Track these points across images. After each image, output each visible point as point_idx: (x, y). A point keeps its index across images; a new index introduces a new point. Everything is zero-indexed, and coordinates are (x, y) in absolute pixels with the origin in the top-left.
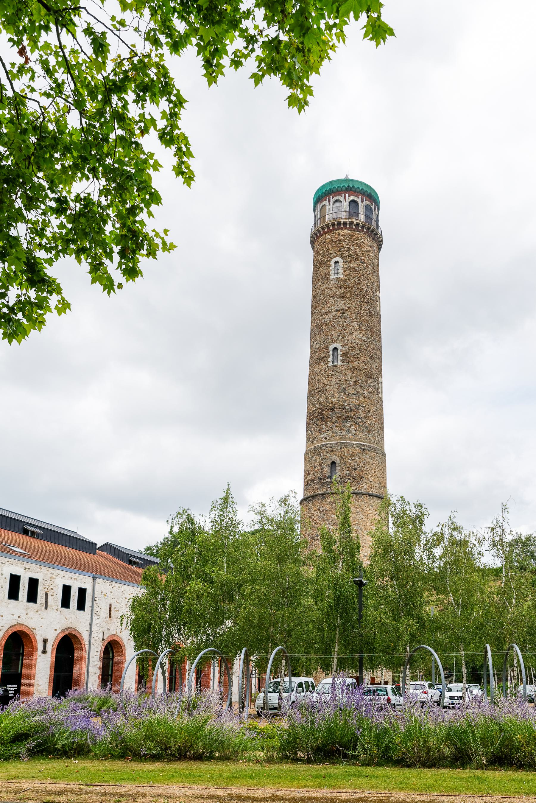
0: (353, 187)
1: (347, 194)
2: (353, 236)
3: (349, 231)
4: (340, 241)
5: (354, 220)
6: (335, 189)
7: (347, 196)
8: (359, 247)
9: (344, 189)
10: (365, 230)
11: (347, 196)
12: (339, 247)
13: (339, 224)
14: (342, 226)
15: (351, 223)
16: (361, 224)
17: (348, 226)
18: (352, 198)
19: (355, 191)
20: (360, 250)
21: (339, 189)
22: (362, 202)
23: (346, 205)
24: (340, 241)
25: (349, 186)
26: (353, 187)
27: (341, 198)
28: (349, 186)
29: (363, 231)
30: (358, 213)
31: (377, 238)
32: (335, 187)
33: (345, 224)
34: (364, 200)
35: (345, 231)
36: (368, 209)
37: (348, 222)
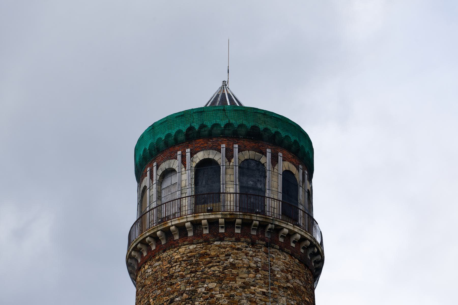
0: (203, 126)
1: (188, 150)
2: (203, 256)
3: (191, 247)
4: (171, 276)
5: (201, 216)
6: (162, 143)
7: (188, 155)
8: (220, 281)
9: (181, 137)
10: (254, 233)
11: (188, 155)
12: (169, 294)
13: (167, 232)
14: (177, 237)
15: (196, 224)
16: (221, 221)
17: (190, 234)
18: (200, 156)
19: (210, 136)
20: (222, 291)
21: (171, 140)
22: (274, 161)
23: (185, 178)
24: (171, 276)
25: (191, 129)
26: (203, 126)
27: (175, 164)
28: (191, 129)
29: (233, 234)
30: (219, 193)
31: (305, 248)
32: (160, 139)
33: (181, 228)
34: (280, 159)
35: (182, 250)
36: (289, 182)
37: (188, 224)
